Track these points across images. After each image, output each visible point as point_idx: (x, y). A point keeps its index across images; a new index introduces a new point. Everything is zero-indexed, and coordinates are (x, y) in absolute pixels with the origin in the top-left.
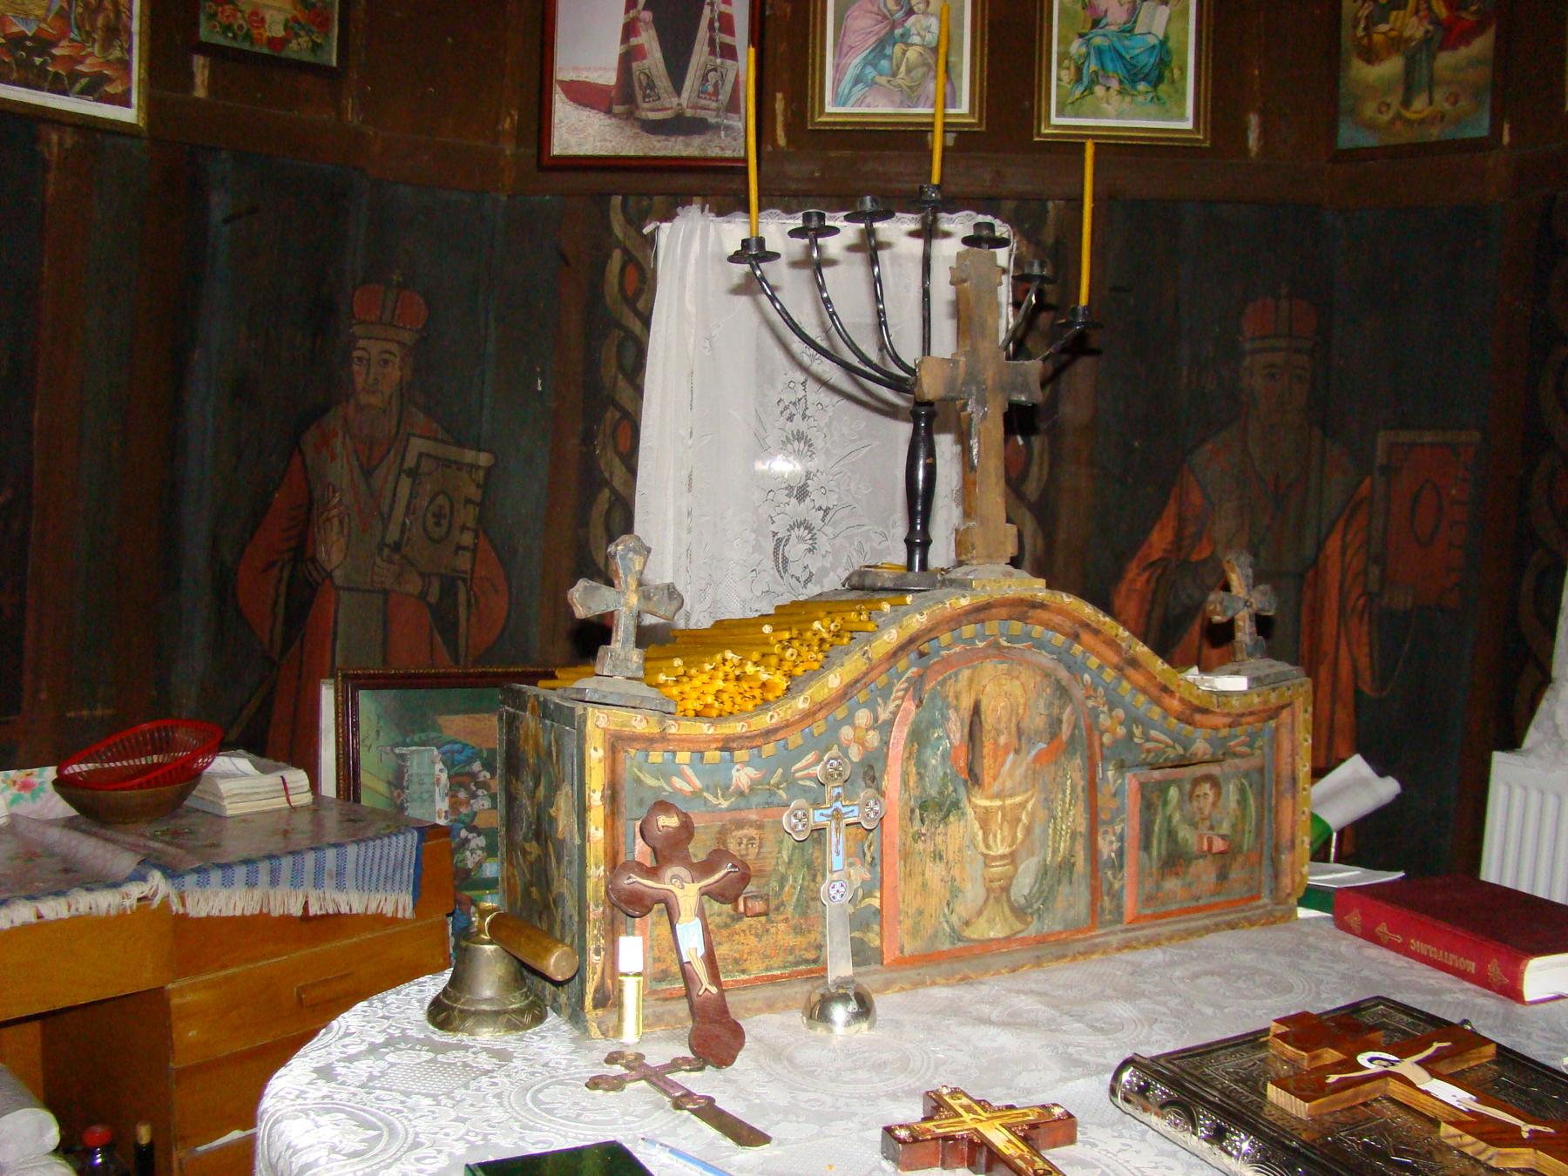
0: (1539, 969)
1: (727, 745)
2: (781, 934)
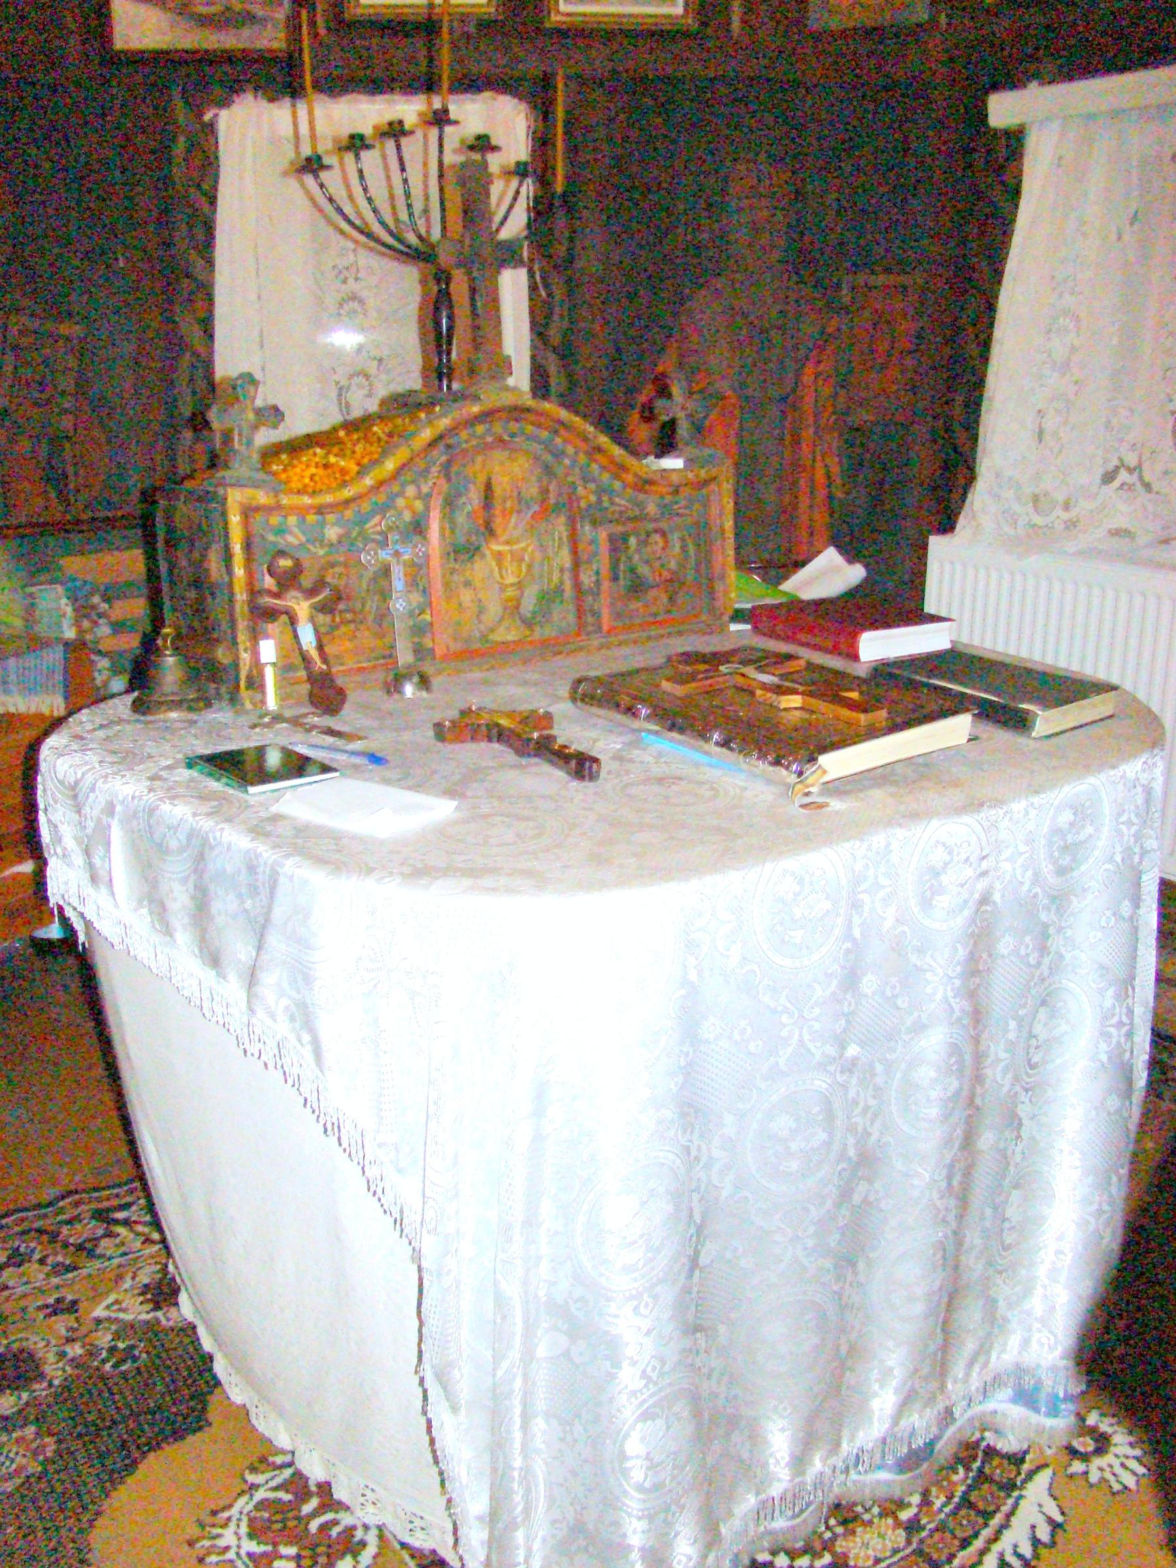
0: (871, 640)
1: (320, 510)
2: (366, 638)
